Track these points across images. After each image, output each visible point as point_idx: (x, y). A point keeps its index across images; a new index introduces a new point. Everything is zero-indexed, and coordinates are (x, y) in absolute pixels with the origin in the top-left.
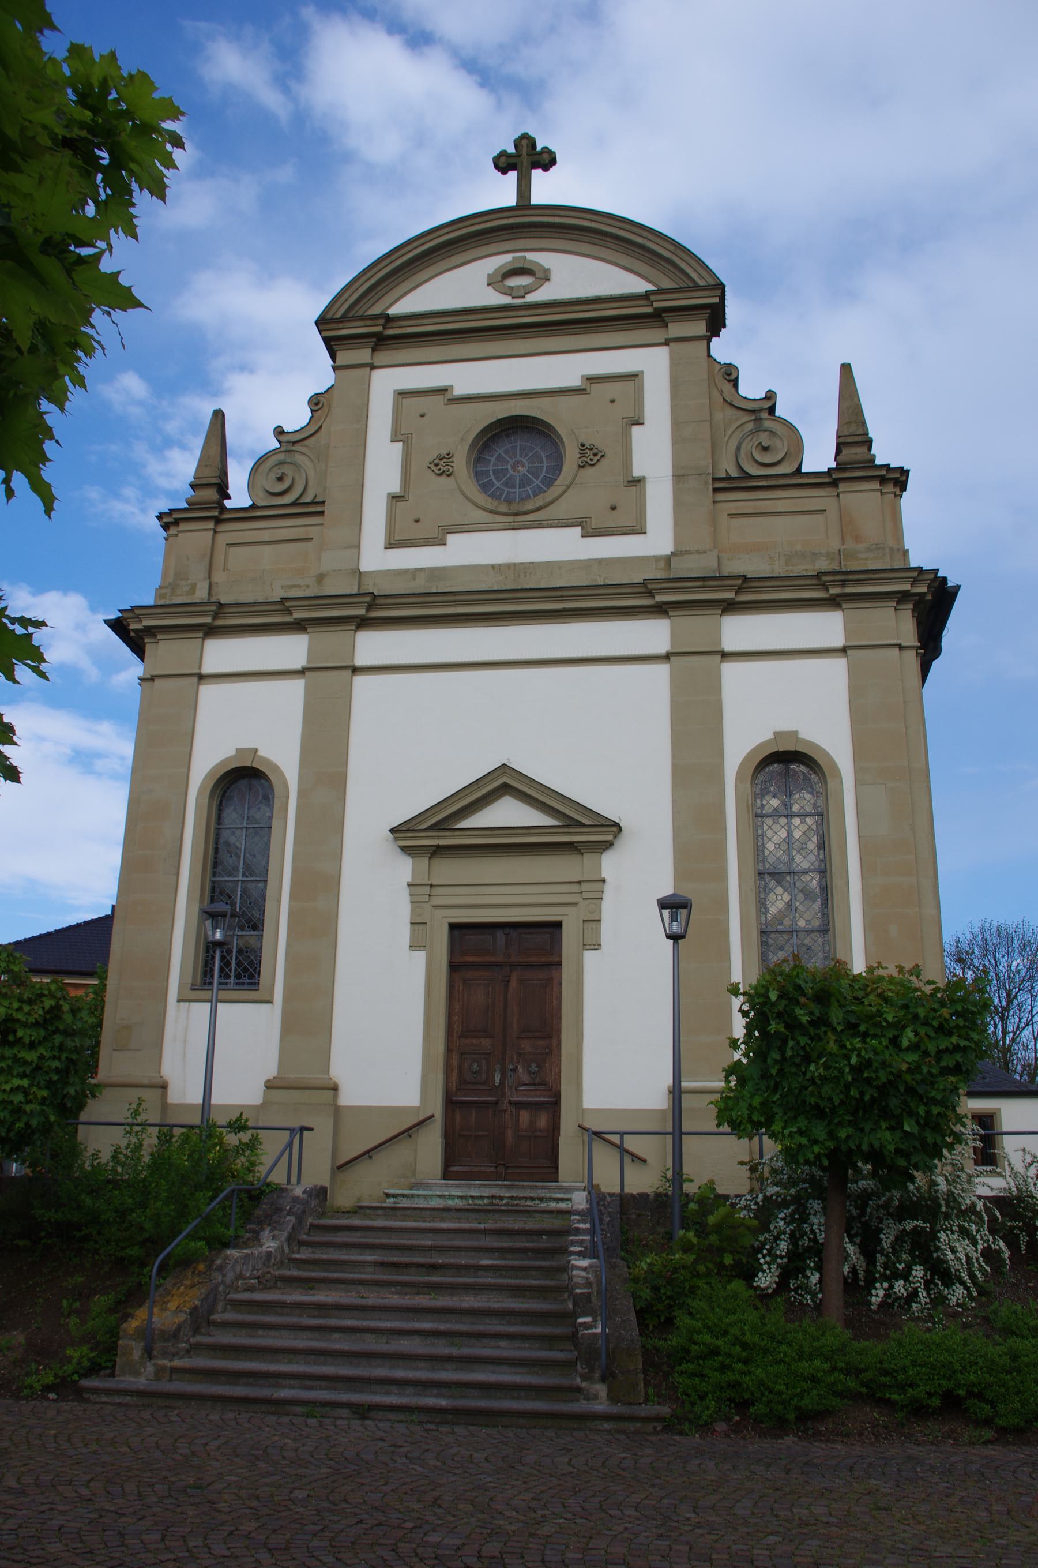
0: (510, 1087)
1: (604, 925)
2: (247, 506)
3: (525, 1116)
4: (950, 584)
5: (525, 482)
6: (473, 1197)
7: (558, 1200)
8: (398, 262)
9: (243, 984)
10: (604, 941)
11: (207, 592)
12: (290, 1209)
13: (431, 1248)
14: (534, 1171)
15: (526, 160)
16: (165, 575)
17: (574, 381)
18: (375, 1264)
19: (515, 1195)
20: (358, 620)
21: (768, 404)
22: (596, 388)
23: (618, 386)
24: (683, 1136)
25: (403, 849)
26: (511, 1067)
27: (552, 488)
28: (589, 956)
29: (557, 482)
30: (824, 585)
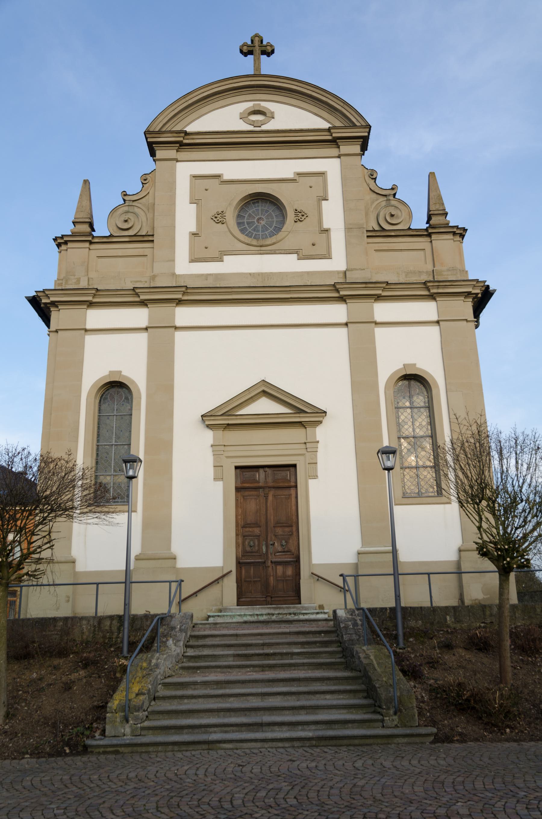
0: (271, 554)
1: (319, 465)
2: (108, 235)
3: (280, 569)
4: (491, 289)
5: (265, 228)
6: (257, 615)
7: (304, 614)
8: (190, 102)
9: (118, 502)
10: (319, 474)
11: (87, 283)
12: (180, 627)
13: (263, 645)
14: (286, 598)
15: (257, 50)
16: (59, 273)
17: (290, 175)
18: (235, 656)
19: (280, 612)
20: (177, 301)
21: (393, 192)
22: (302, 180)
23: (313, 179)
24: (392, 572)
25: (208, 426)
26: (271, 543)
27: (280, 233)
28: (311, 482)
29: (283, 230)
30: (427, 288)
